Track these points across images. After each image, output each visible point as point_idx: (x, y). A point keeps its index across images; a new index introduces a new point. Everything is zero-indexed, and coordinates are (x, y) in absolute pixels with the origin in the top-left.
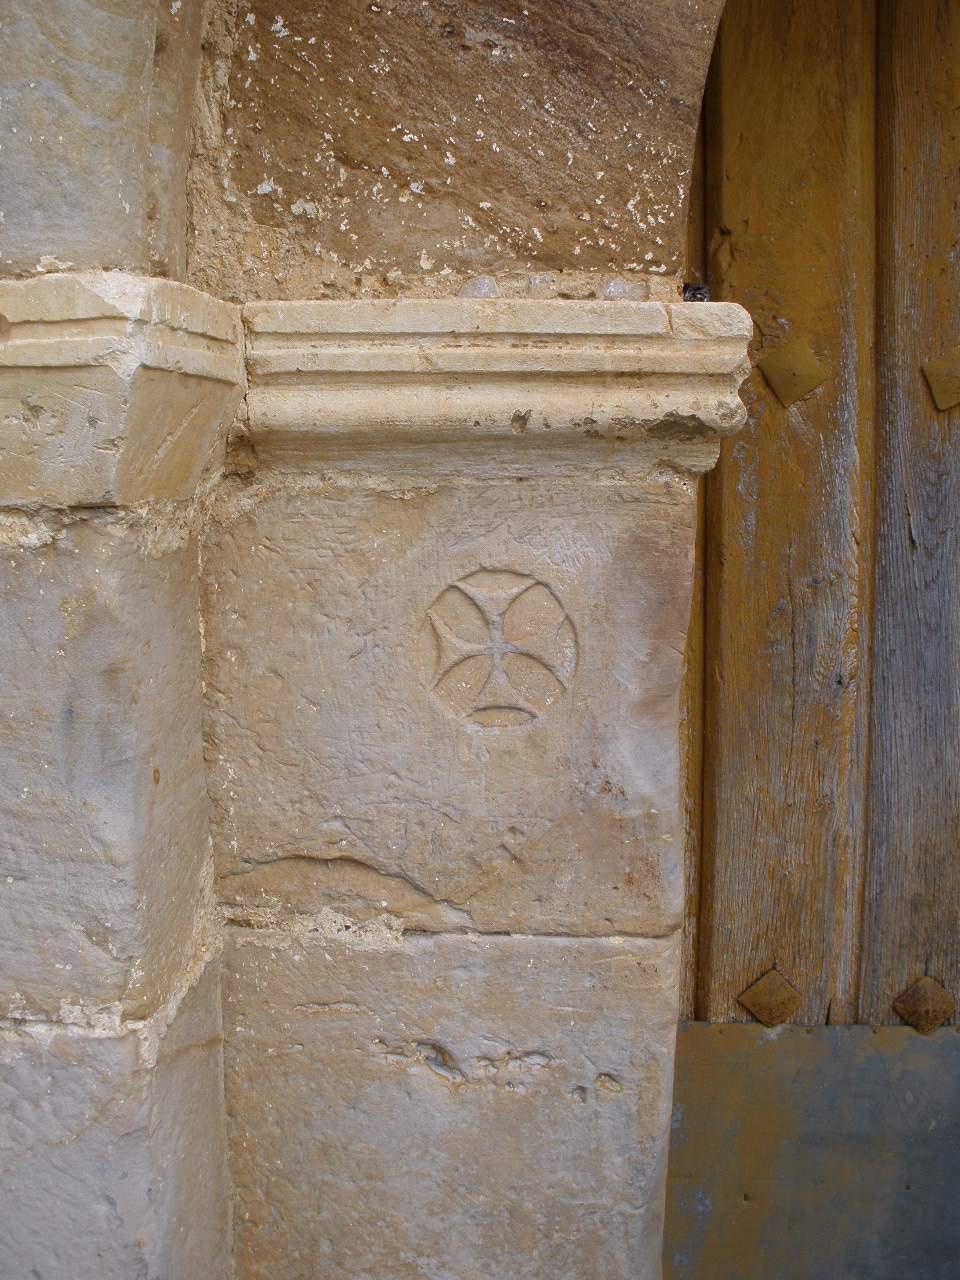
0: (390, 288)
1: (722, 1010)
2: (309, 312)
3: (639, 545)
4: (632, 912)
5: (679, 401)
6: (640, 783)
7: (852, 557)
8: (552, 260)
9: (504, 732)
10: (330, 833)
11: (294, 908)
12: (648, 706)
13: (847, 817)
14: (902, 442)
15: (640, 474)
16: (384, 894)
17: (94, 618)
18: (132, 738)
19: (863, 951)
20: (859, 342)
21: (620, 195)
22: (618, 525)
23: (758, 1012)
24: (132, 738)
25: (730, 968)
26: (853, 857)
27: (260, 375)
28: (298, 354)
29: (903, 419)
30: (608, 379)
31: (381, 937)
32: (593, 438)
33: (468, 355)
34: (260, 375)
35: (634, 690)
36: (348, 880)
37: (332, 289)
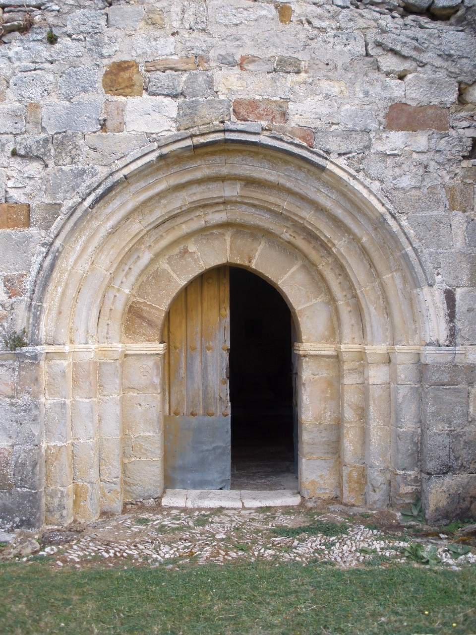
0: (137, 343)
1: (172, 414)
2: (131, 345)
3: (155, 363)
4: (156, 392)
5: (158, 352)
6: (156, 381)
7: (183, 365)
8: (149, 341)
9: (145, 377)
10: (131, 386)
11: (128, 392)
12: (157, 375)
13: (184, 393)
14: (188, 353)
15: (155, 357)
16: (136, 391)
17: (117, 367)
18: (119, 375)
19: (187, 407)
20: (184, 344)
21: (154, 336)
22: (153, 361)
23: (176, 414)
24: (119, 375)
25: (173, 409)
26: (186, 397)
27: (127, 350)
28: (130, 348)
29: (188, 351)
30: (330, 260)
31: (135, 394)
32: (153, 355)
33: (142, 349)
34: (127, 350)
35: (155, 374)
36: (133, 390)
37: (132, 343)
